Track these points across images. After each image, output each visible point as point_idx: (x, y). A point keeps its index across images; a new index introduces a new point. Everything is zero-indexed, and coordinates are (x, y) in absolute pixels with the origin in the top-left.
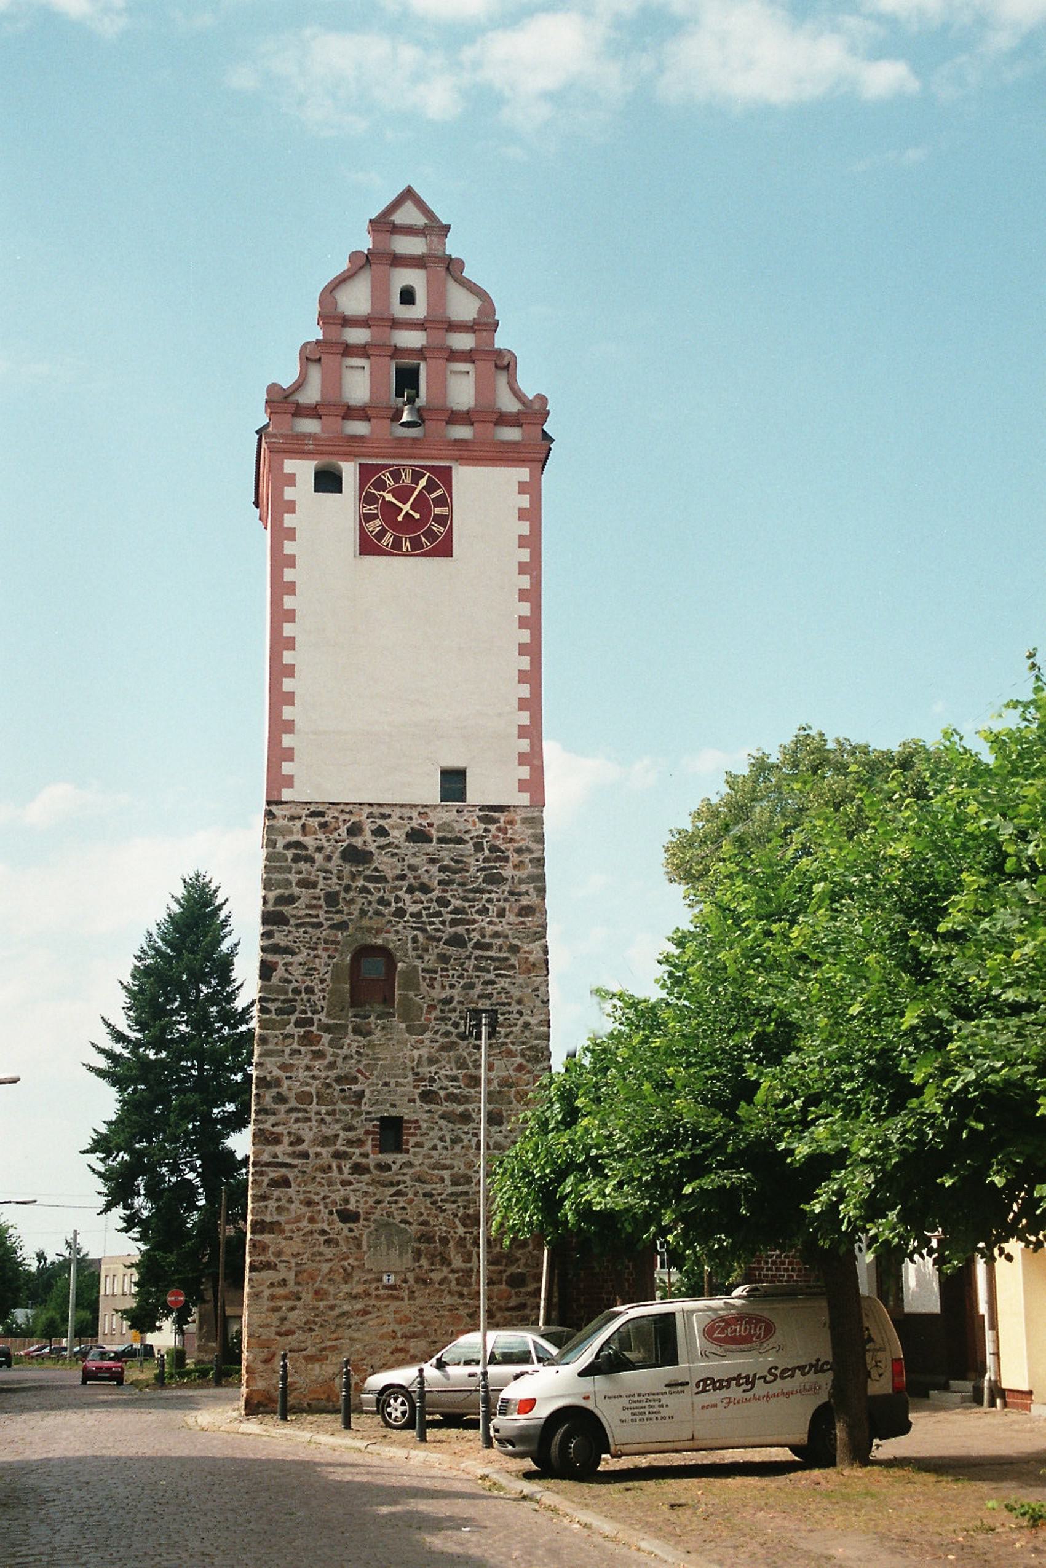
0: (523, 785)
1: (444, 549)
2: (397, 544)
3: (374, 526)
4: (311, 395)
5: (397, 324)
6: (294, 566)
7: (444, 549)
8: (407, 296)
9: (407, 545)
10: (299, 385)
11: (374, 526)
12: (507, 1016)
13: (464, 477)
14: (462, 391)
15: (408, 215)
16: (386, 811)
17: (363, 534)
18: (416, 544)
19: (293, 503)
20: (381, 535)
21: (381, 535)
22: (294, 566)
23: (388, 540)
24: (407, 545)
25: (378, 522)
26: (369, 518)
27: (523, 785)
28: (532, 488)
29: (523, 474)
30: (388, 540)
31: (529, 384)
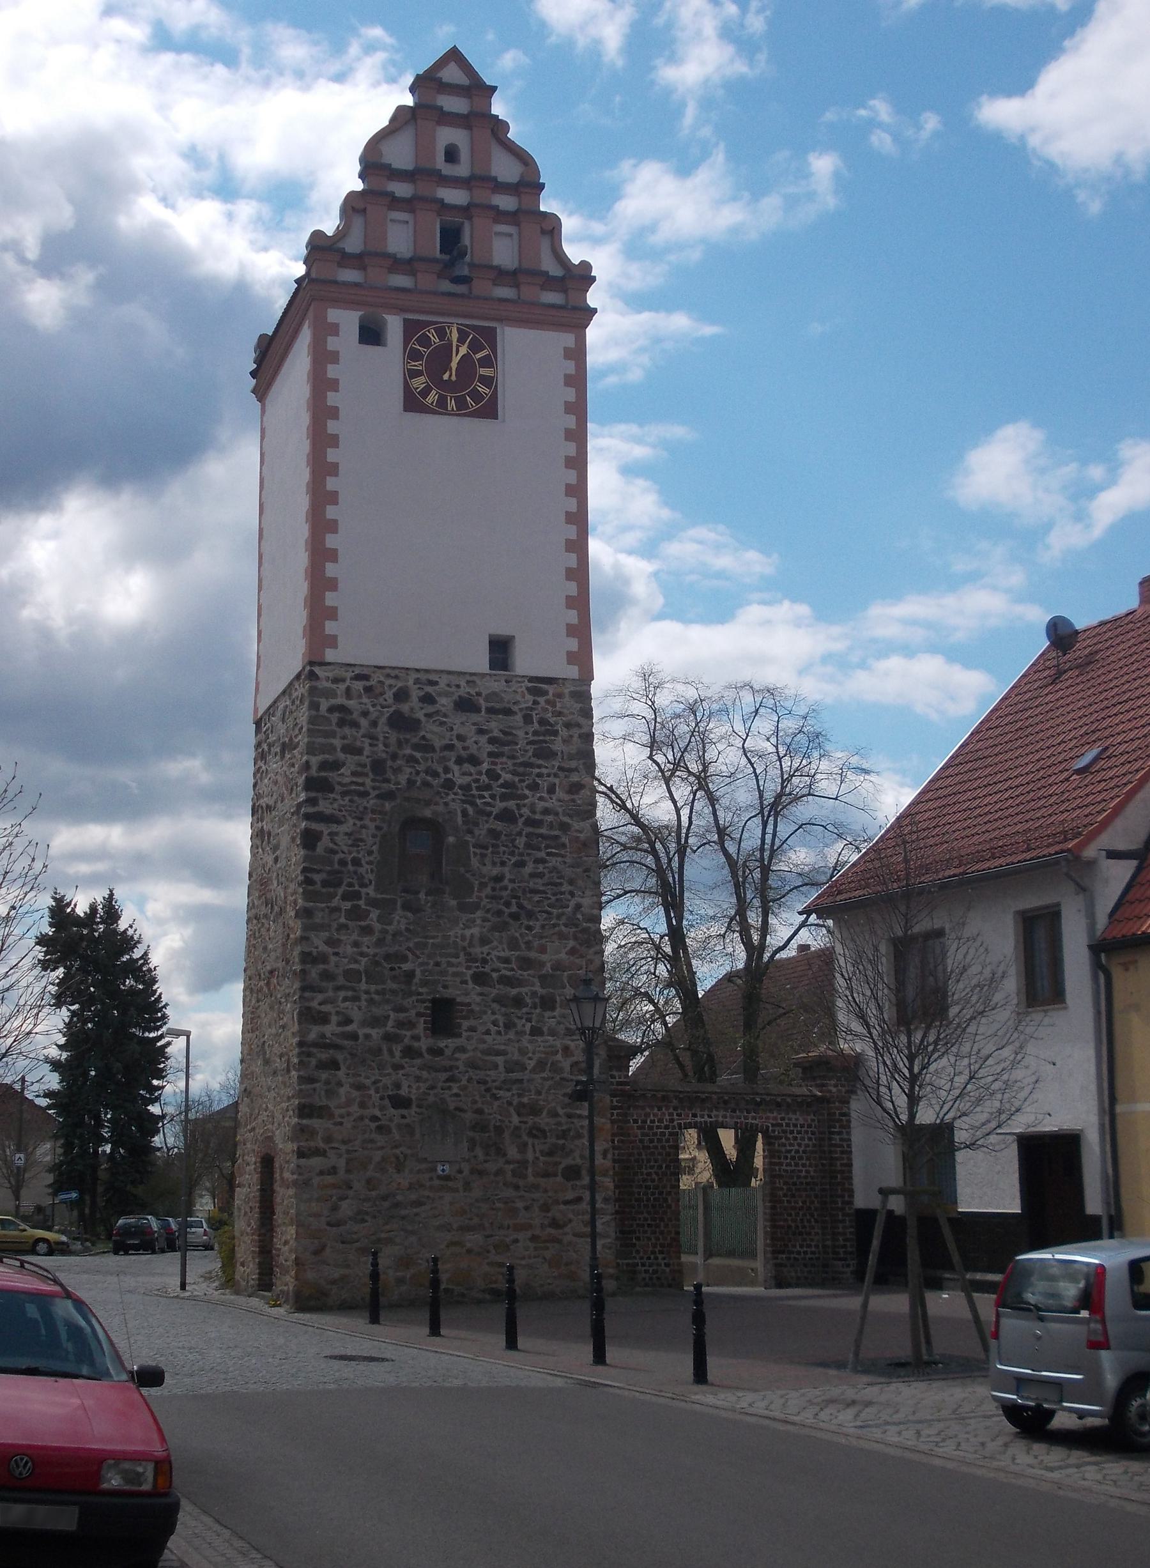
1: (489, 410)
2: (442, 402)
3: (419, 383)
7: (489, 410)
8: (451, 155)
9: (452, 404)
11: (419, 383)
17: (408, 390)
18: (461, 404)
21: (425, 392)
23: (432, 398)
24: (452, 404)
25: (422, 379)
30: (432, 398)
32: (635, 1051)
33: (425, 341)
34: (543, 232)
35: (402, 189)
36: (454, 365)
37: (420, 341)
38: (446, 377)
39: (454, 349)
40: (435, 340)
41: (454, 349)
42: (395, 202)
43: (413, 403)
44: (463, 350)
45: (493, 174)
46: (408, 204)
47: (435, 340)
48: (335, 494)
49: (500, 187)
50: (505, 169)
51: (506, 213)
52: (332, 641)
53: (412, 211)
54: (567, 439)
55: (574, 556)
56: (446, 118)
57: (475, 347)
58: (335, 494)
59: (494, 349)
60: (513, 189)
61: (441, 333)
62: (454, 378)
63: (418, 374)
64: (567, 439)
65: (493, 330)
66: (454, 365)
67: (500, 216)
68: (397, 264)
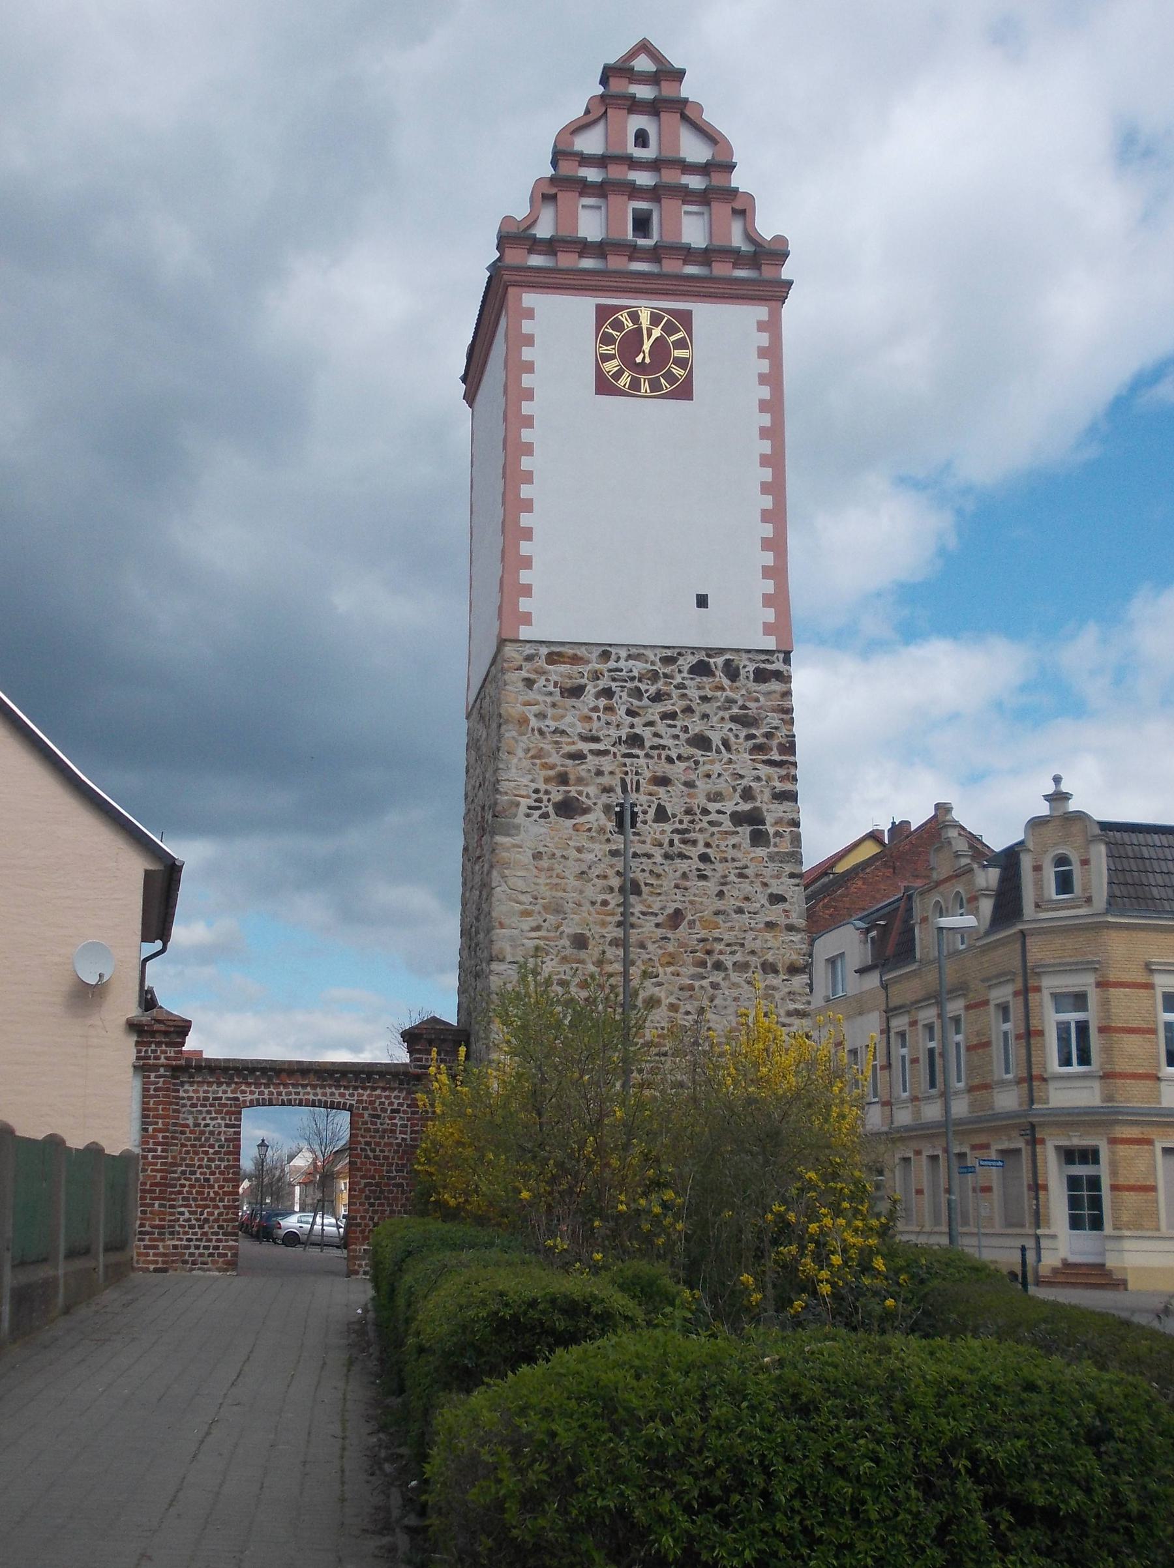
0: (768, 629)
1: (684, 391)
2: (635, 385)
3: (611, 367)
4: (543, 231)
5: (634, 164)
6: (762, 484)
7: (684, 391)
8: (641, 139)
9: (645, 387)
10: (532, 221)
11: (611, 367)
12: (519, 778)
13: (704, 314)
14: (693, 230)
15: (643, 64)
16: (581, 652)
17: (599, 373)
18: (655, 386)
19: (762, 410)
20: (618, 375)
21: (618, 375)
22: (762, 484)
23: (624, 381)
24: (645, 387)
25: (615, 362)
26: (606, 358)
27: (768, 629)
28: (772, 326)
29: (761, 312)
30: (624, 381)
31: (767, 227)
32: (873, 1557)
33: (617, 325)
34: (735, 212)
35: (592, 175)
36: (646, 347)
37: (613, 326)
38: (639, 359)
39: (645, 332)
40: (629, 325)
41: (645, 332)
42: (584, 188)
43: (604, 386)
44: (657, 332)
45: (682, 155)
46: (601, 190)
47: (629, 325)
48: (530, 474)
49: (688, 168)
50: (694, 150)
51: (693, 192)
52: (761, 326)
53: (604, 196)
54: (760, 384)
55: (766, 362)
56: (634, 106)
57: (670, 329)
58: (530, 474)
59: (689, 332)
60: (704, 169)
61: (635, 317)
62: (647, 360)
63: (610, 357)
64: (760, 384)
65: (689, 313)
66: (646, 347)
67: (687, 195)
68: (584, 248)
